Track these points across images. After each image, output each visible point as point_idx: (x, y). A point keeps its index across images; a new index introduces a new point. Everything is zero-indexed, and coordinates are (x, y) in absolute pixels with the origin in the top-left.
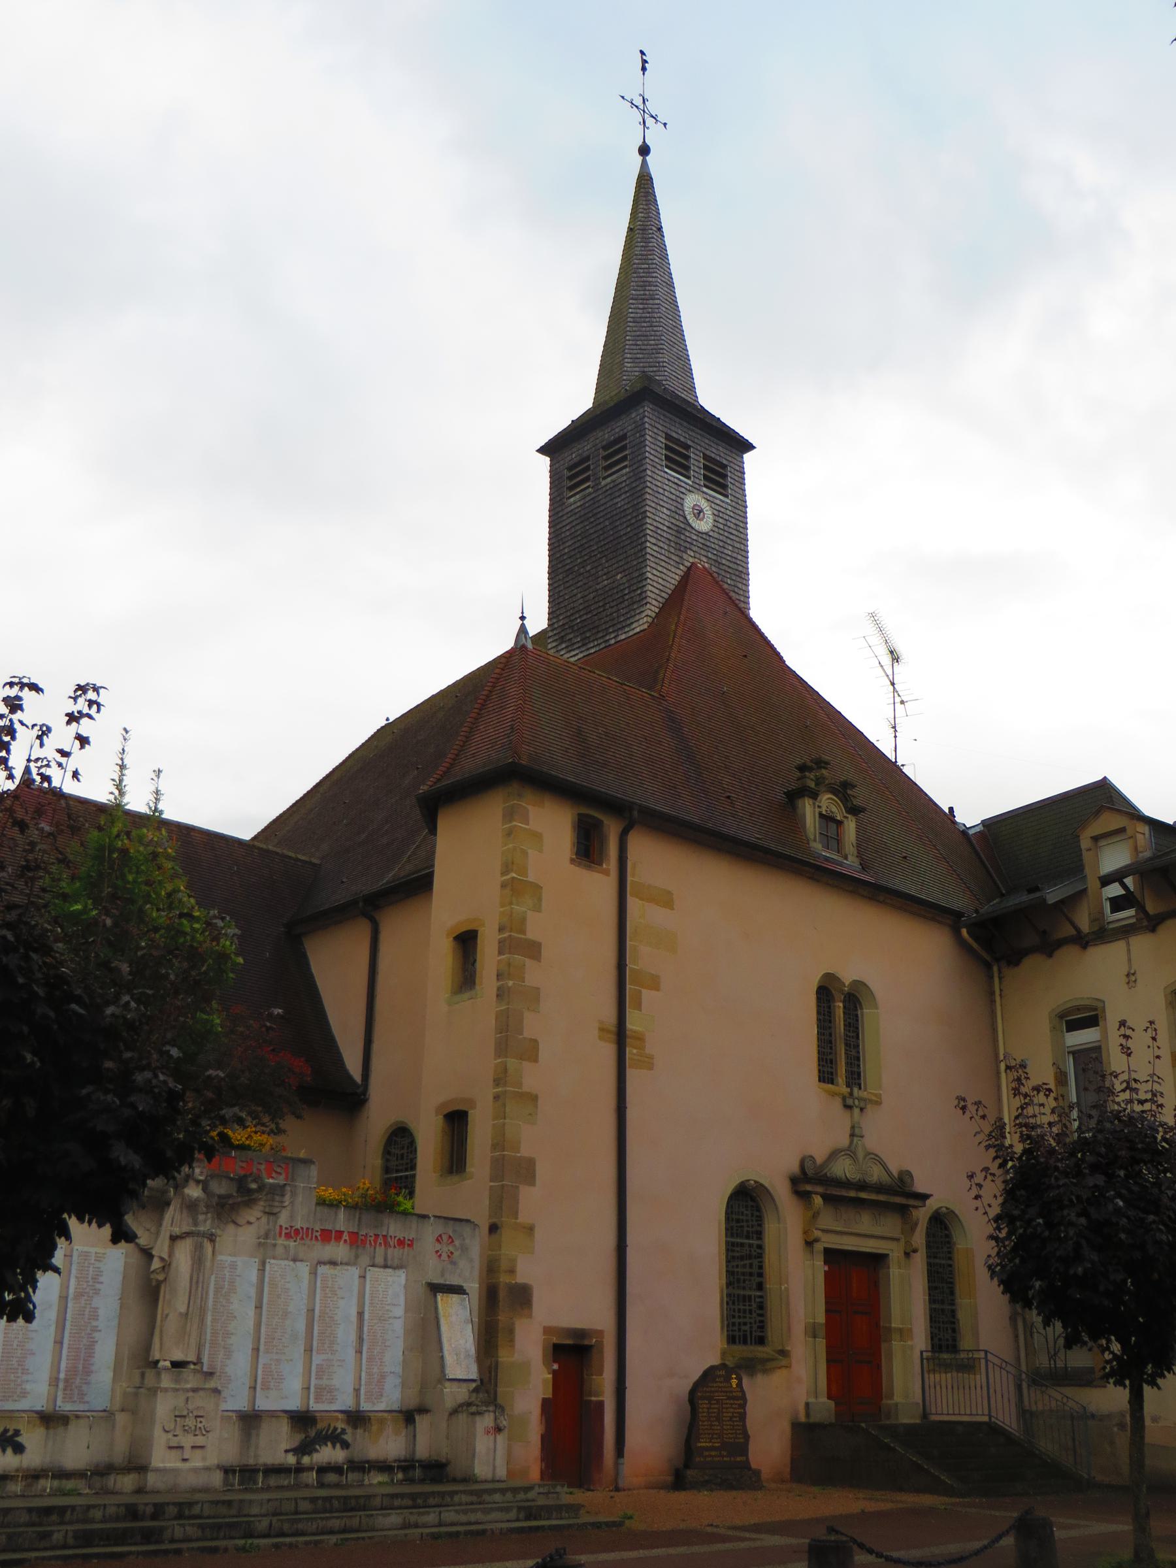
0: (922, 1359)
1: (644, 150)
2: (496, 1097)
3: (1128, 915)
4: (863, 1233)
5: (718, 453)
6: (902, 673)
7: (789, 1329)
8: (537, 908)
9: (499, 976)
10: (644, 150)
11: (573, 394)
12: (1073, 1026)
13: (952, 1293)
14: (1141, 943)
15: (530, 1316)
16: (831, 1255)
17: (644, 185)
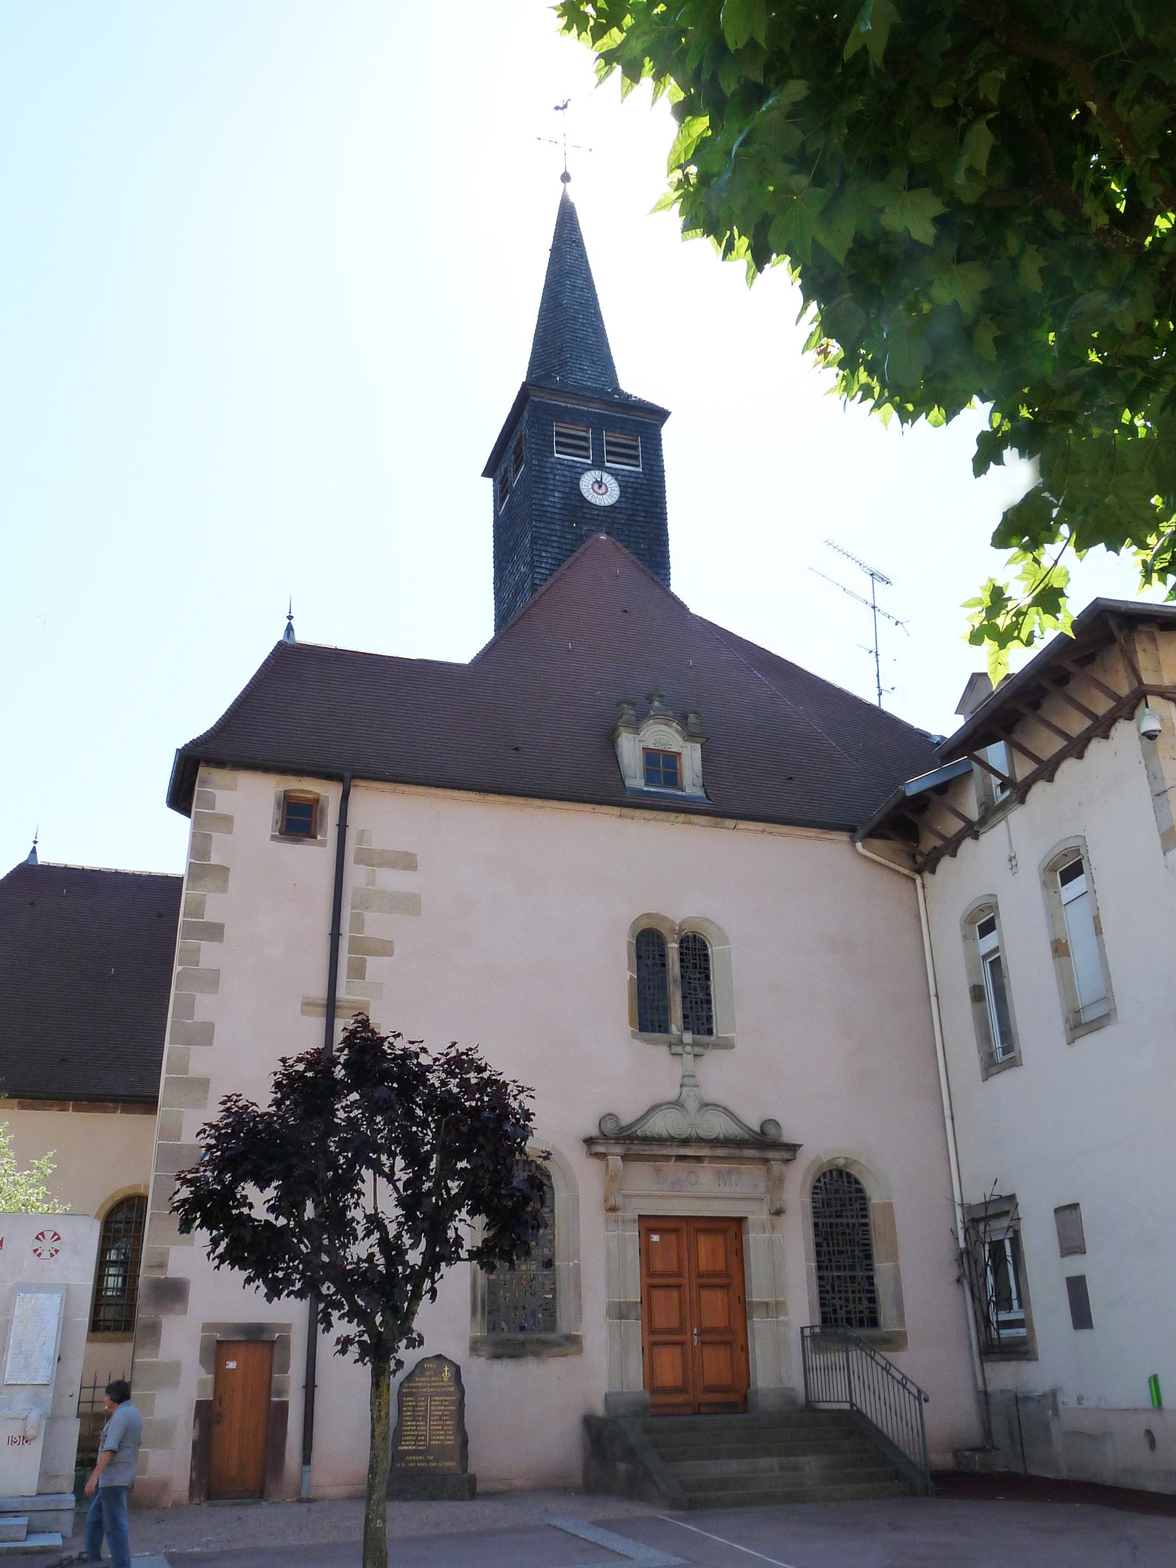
0: (803, 1337)
4: (705, 1192)
5: (637, 429)
7: (579, 1309)
13: (869, 1256)
15: (185, 1312)
16: (649, 1224)
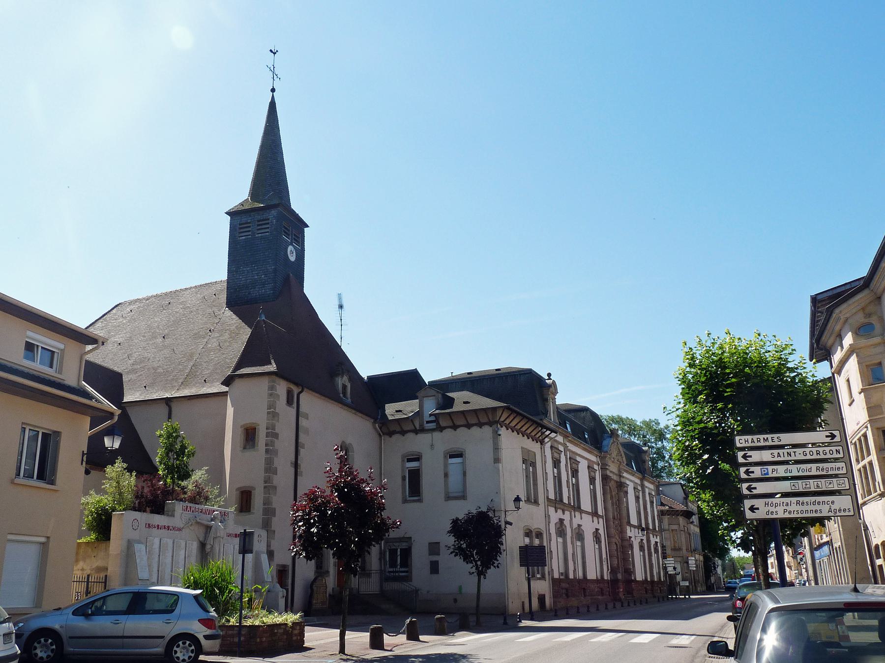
1: (273, 90)
2: (265, 487)
3: (432, 426)
5: (295, 227)
6: (345, 312)
8: (278, 421)
9: (266, 445)
10: (273, 90)
11: (239, 192)
12: (409, 460)
14: (436, 435)
17: (272, 106)
